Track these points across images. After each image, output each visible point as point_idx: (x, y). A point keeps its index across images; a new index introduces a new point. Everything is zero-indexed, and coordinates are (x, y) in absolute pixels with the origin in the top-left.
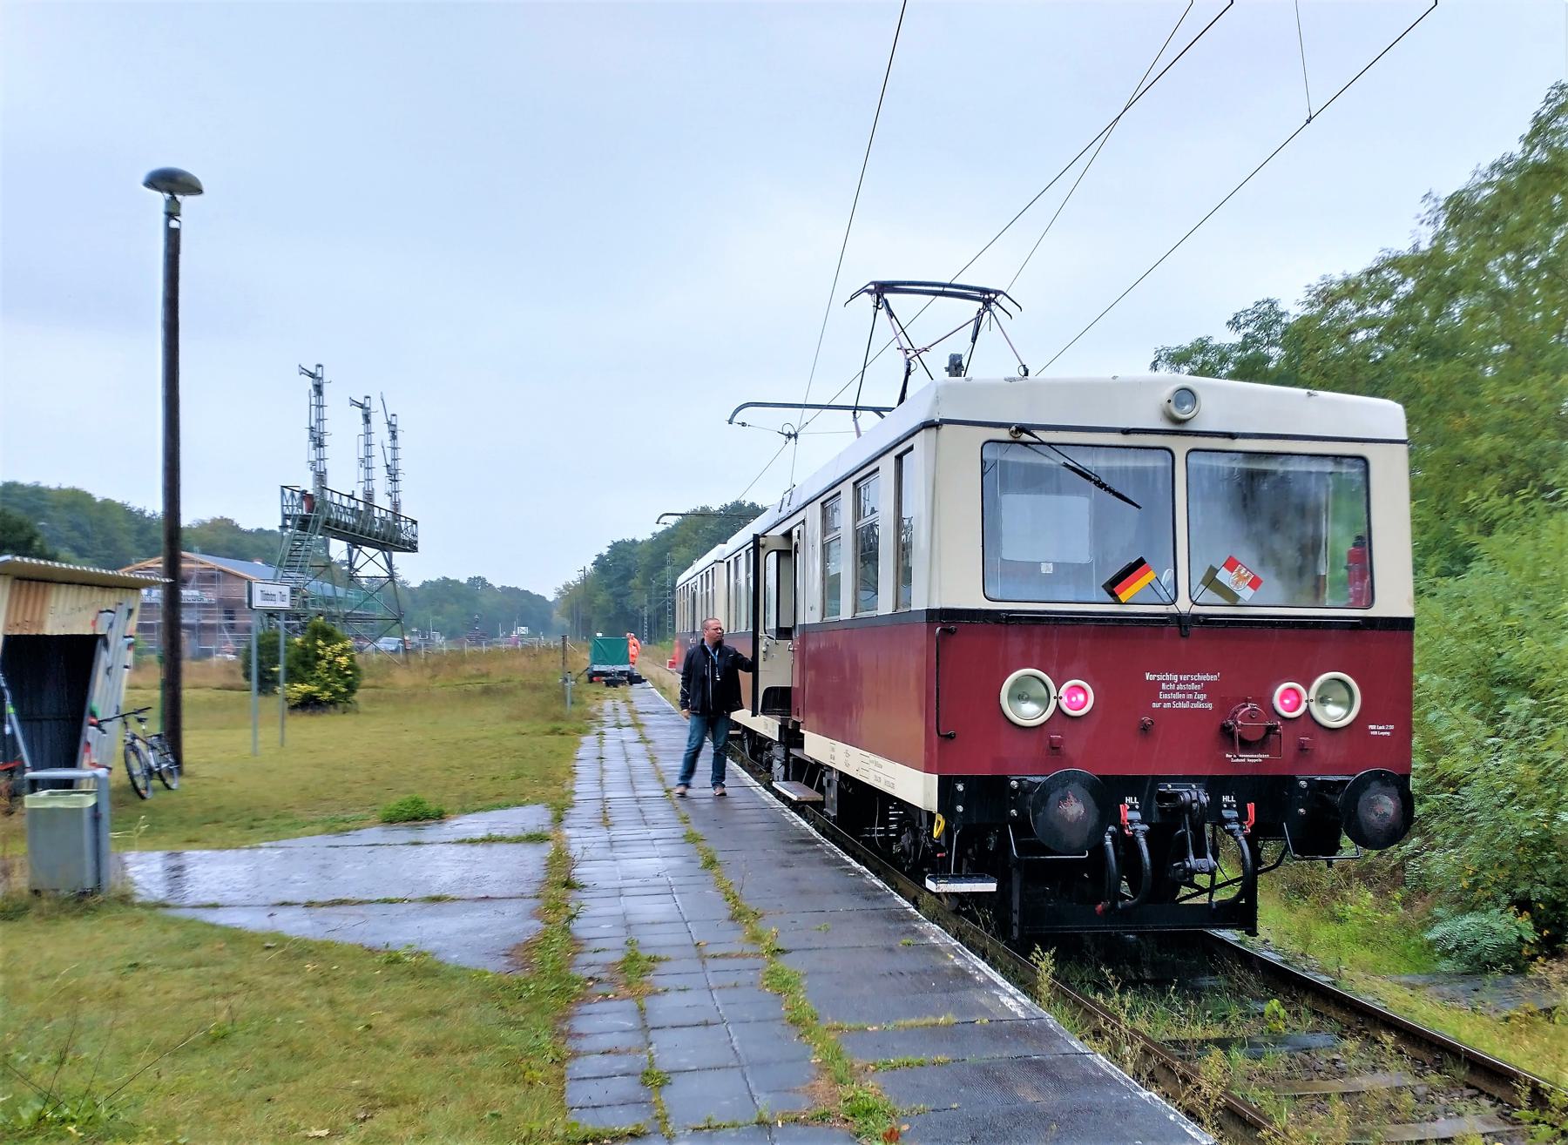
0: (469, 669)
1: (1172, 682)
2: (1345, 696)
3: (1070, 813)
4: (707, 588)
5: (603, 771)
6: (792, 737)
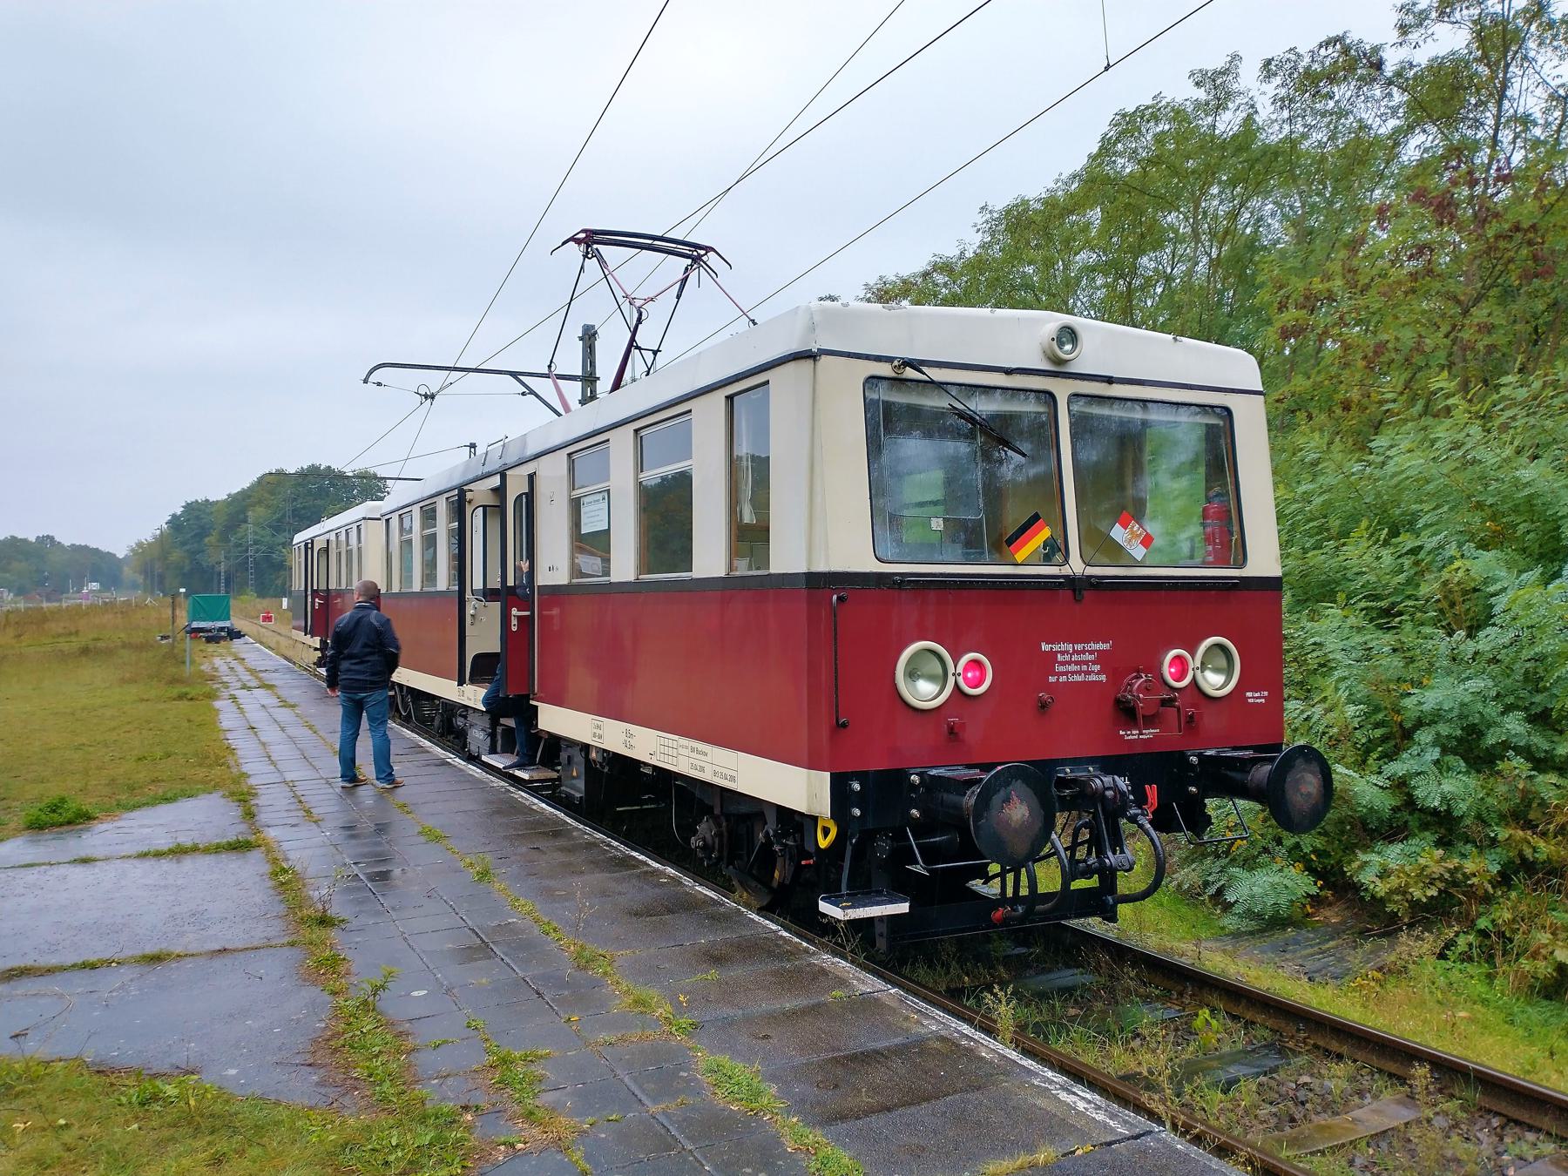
0: (55, 627)
1: (1067, 652)
2: (1223, 663)
3: (1015, 818)
5: (264, 744)
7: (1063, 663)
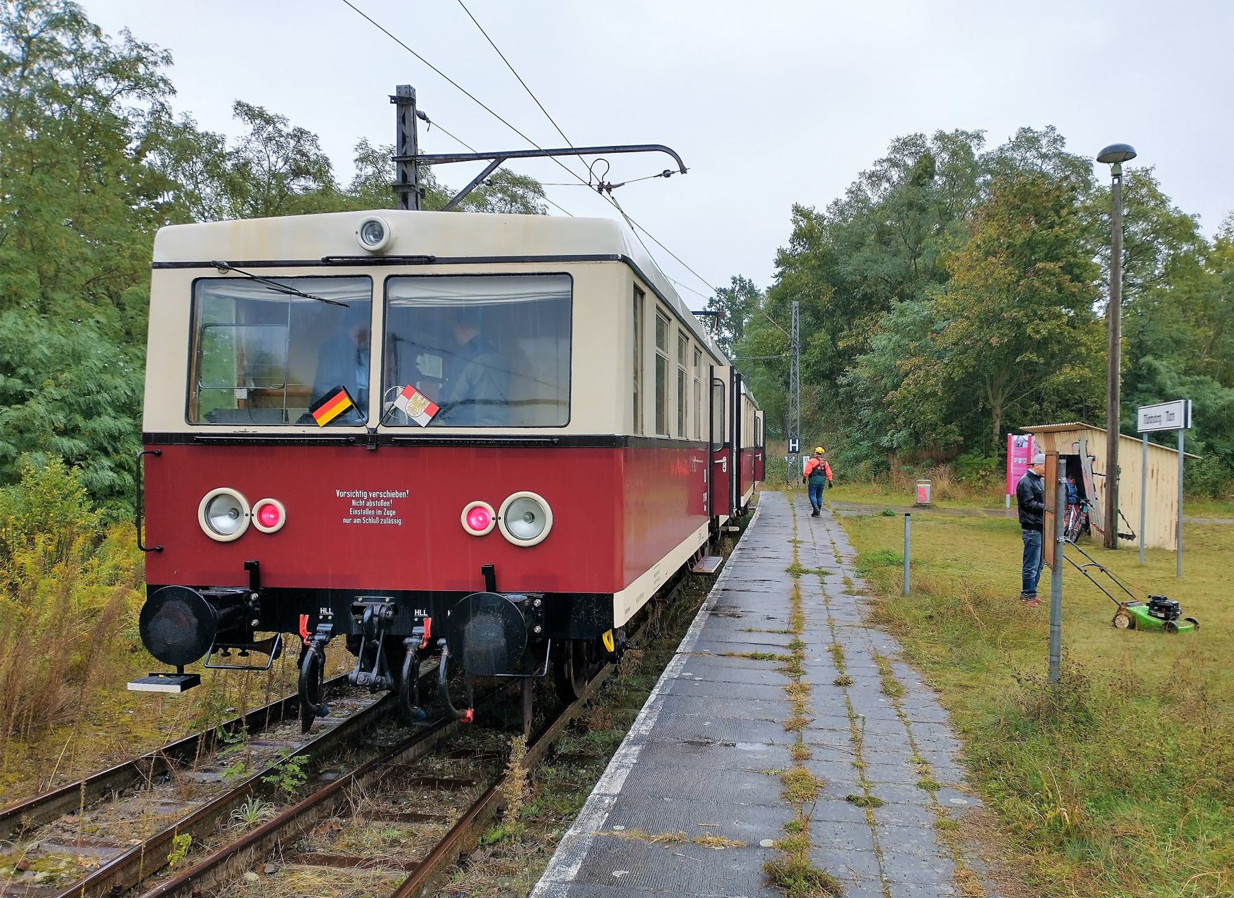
1: (362, 499)
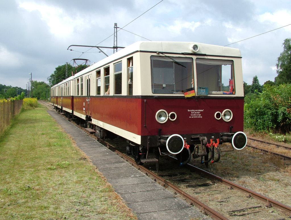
1: (194, 112)
4: (66, 86)
6: (89, 119)
7: (192, 114)
